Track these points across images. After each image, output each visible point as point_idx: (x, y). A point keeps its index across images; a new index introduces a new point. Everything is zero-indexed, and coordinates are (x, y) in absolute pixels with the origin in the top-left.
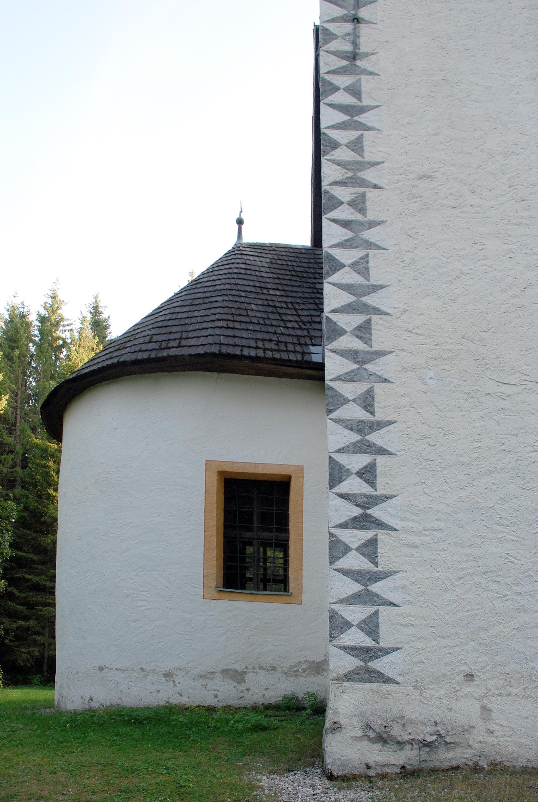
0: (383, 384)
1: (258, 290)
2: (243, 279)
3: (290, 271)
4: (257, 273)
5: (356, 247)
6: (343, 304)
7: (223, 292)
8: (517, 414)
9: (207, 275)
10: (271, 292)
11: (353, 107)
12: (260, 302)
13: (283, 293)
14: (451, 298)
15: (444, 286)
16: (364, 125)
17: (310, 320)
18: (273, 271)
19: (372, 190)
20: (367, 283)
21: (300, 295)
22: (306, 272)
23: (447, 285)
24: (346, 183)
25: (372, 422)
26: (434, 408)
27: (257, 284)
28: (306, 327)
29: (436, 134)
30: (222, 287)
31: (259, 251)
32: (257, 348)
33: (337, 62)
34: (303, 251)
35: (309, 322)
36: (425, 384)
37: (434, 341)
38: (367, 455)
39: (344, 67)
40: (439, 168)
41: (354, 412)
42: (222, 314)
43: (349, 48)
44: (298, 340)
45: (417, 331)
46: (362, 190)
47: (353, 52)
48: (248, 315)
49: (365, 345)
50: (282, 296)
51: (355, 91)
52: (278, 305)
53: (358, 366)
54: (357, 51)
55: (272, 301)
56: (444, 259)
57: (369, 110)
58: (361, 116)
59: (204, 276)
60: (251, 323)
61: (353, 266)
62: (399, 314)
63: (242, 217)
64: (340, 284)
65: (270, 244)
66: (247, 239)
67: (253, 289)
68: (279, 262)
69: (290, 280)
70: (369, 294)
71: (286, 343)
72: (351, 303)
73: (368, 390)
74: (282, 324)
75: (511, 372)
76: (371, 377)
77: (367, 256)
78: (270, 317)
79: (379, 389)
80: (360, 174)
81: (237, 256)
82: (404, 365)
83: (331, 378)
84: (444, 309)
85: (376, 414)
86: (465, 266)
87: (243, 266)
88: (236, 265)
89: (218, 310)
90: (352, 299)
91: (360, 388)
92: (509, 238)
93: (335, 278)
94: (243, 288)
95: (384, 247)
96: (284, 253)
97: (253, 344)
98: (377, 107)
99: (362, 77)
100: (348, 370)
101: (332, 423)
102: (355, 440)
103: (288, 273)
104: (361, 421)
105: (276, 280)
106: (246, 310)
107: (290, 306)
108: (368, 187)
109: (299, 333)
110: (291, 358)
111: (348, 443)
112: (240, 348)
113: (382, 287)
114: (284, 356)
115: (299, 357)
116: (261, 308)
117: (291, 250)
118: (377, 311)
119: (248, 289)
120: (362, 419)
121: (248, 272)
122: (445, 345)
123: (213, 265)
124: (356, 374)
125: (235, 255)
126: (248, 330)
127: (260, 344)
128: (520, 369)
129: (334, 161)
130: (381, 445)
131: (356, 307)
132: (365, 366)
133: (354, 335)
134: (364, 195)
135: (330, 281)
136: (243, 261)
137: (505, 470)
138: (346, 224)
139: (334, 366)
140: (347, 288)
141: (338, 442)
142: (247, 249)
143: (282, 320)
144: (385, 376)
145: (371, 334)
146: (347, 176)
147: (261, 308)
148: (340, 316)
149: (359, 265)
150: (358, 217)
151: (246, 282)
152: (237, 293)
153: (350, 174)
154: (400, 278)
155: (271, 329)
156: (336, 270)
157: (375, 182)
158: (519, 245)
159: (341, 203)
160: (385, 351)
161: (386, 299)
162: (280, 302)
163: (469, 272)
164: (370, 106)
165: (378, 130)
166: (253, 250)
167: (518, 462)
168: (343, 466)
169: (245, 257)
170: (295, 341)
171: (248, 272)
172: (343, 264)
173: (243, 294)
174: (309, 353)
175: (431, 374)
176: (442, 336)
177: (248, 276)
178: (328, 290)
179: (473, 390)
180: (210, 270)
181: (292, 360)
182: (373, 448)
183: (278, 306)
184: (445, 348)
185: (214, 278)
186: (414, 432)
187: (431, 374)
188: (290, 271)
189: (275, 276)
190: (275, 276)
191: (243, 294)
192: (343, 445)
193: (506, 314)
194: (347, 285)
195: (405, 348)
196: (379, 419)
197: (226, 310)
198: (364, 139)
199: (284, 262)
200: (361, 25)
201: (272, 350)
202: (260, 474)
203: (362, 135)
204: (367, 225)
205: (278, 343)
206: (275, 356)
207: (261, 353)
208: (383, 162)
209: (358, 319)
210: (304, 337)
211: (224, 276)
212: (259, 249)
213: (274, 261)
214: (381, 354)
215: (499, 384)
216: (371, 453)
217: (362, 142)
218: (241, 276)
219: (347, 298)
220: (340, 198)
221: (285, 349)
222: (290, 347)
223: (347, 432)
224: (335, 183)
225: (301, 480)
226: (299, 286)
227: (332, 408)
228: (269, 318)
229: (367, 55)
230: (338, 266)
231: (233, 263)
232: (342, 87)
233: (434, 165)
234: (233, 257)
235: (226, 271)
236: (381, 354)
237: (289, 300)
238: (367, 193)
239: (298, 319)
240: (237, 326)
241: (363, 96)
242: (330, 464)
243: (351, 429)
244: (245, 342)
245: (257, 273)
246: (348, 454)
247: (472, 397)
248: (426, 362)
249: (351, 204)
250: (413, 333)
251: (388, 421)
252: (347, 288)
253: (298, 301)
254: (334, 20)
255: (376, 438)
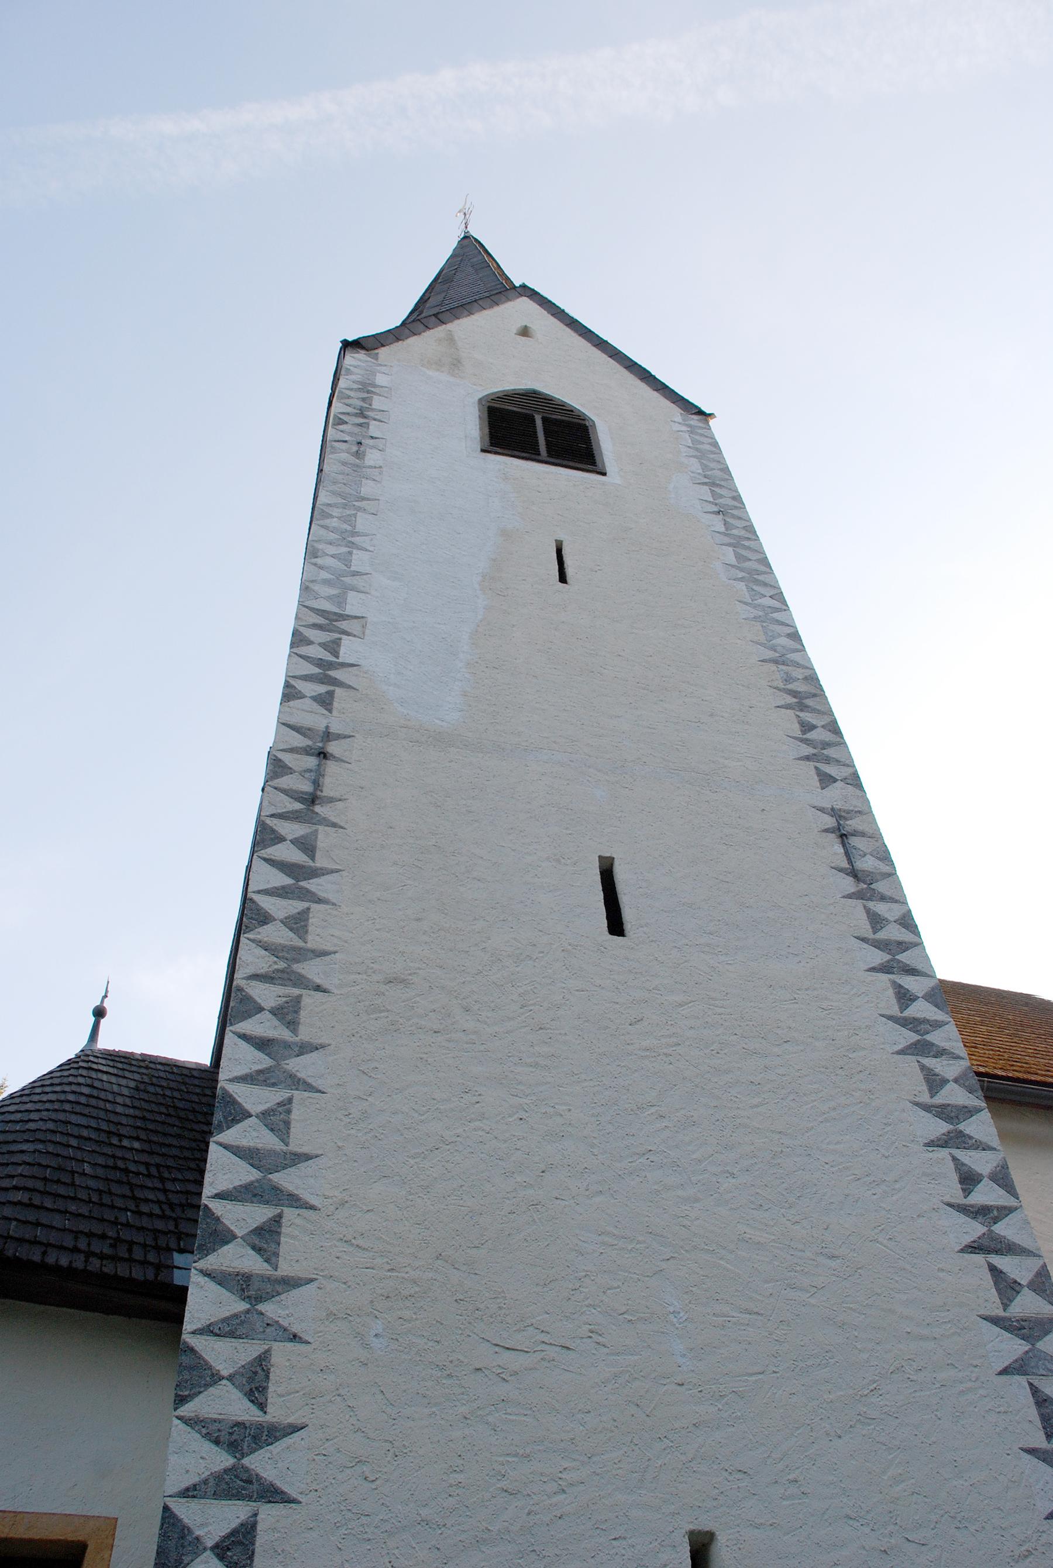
0: (290, 1345)
1: (103, 1137)
2: (81, 1114)
3: (167, 1107)
4: (108, 1106)
5: (274, 1085)
6: (237, 1183)
7: (40, 1136)
8: (529, 1412)
9: (17, 1100)
10: (126, 1143)
11: (300, 867)
12: (101, 1160)
13: (146, 1147)
14: (422, 1183)
15: (412, 1162)
16: (313, 894)
17: (184, 1202)
18: (137, 1103)
19: (312, 993)
20: (285, 1148)
21: (174, 1152)
22: (194, 1111)
23: (417, 1160)
24: (273, 978)
25: (260, 1427)
26: (380, 1397)
27: (104, 1126)
28: (174, 1215)
29: (418, 920)
30: (40, 1125)
31: (120, 1065)
32: (75, 1250)
33: (287, 804)
34: (195, 1073)
35: (181, 1205)
36: (366, 1346)
37: (388, 1263)
38: (241, 1502)
39: (296, 811)
40: (420, 969)
41: (226, 1403)
42: (25, 1176)
43: (307, 787)
44: (156, 1239)
45: (360, 1242)
46: (296, 991)
47: (311, 794)
48: (73, 1184)
49: (266, 1264)
50: (143, 1151)
51: (307, 846)
52: (132, 1167)
53: (248, 1306)
54: (319, 793)
55: (123, 1159)
56: (416, 1115)
57: (323, 875)
58: (311, 881)
59: (14, 1101)
60: (74, 1199)
61: (265, 1116)
62: (332, 1208)
63: (105, 1005)
64: (238, 1147)
65: (142, 1054)
66: (104, 1043)
67: (94, 1135)
68: (151, 1089)
69: (163, 1123)
70: (284, 1168)
71: (131, 1244)
72: (251, 1183)
73: (260, 1356)
74: (131, 1205)
75: (518, 1327)
76: (269, 1330)
77: (290, 1100)
78: (113, 1190)
79: (282, 1354)
80: (297, 967)
81: (81, 1071)
82: (332, 1308)
83: (195, 1327)
84: (409, 1203)
85: (269, 1409)
86: (447, 1128)
87: (86, 1090)
88: (74, 1088)
89: (20, 1170)
90: (253, 1175)
91: (244, 1352)
92: (519, 1087)
93: (231, 1135)
94: (75, 1131)
95: (320, 1088)
96: (162, 1074)
97: (69, 1242)
98: (337, 871)
99: (321, 828)
100: (228, 1314)
101: (182, 1426)
102: (223, 1466)
103: (163, 1110)
104: (238, 1424)
105: (138, 1120)
106: (73, 1172)
107: (154, 1171)
108: (306, 988)
109: (160, 1225)
110: (134, 1275)
111: (207, 1473)
112: (43, 1249)
113: (308, 1157)
114: (122, 1270)
115: (150, 1275)
116: (100, 1172)
117: (175, 1070)
118: (295, 1201)
119: (85, 1133)
120: (240, 1419)
121: (93, 1102)
122: (407, 1269)
123: (34, 1082)
124: (242, 1323)
125: (78, 1068)
126: (66, 1212)
127: (82, 1244)
128: (534, 1321)
129: (259, 943)
130: (270, 1479)
131: (259, 1191)
132: (260, 1307)
133: (249, 1245)
134: (298, 999)
135: (221, 1140)
136: (89, 1081)
137: (507, 1537)
138: (262, 1044)
139: (205, 1302)
140: (248, 1155)
141: (187, 1471)
142: (100, 1061)
143: (134, 1198)
144: (295, 1328)
145: (279, 1244)
146: (276, 967)
147: (100, 1172)
148: (229, 1205)
149: (274, 1115)
150: (285, 1034)
151: (83, 1121)
152: (64, 1139)
153: (281, 965)
154: (340, 1144)
155: (109, 1215)
156: (235, 1121)
157: (318, 981)
158: (534, 1098)
159: (261, 1009)
160: (300, 1279)
161: (312, 1181)
162: (135, 1162)
163: (454, 1139)
164: (326, 869)
165: (334, 904)
166: (111, 1063)
167: (531, 1517)
168: (189, 1529)
169: (94, 1075)
170: (150, 1241)
171: (93, 1102)
172: (248, 1112)
173: (74, 1142)
174: (168, 1267)
175: (378, 1326)
176: (402, 1253)
177: (92, 1110)
178: (215, 1154)
179: (451, 1362)
180: (26, 1092)
181: (135, 1280)
182: (255, 1487)
183: (133, 1169)
184: (406, 1276)
185: (29, 1106)
186: (338, 1451)
187: (378, 1326)
188: (167, 1107)
189: (137, 1113)
190: (137, 1113)
191: (74, 1142)
192: (196, 1479)
193: (511, 1216)
194: (249, 1149)
195: (337, 1274)
196: (275, 1420)
197: (35, 1171)
198: (311, 915)
199: (159, 1090)
200: (328, 762)
201: (102, 1257)
202: (21, 1540)
203: (308, 909)
204: (296, 1049)
205: (117, 1241)
206: (105, 1270)
207: (79, 1263)
208: (335, 952)
209: (258, 1214)
210: (165, 1233)
211: (48, 1106)
212: (123, 1062)
213: (142, 1086)
214: (291, 1283)
215: (497, 1349)
216: (250, 1498)
217: (307, 920)
218: (78, 1109)
219: (245, 1174)
220: (259, 1001)
221: (126, 1256)
222: (138, 1254)
223: (208, 1447)
224: (255, 977)
225: (106, 1556)
226: (179, 1136)
227: (186, 1393)
228: (110, 1193)
229: (331, 800)
230: (238, 1114)
231: (70, 1084)
232: (290, 837)
233: (411, 964)
234: (72, 1072)
235: (53, 1097)
236: (291, 1283)
237: (157, 1160)
238: (304, 998)
239: (162, 1197)
240: (48, 1203)
241: (318, 854)
242: (162, 1525)
243: (217, 1442)
244: (53, 1238)
245: (108, 1106)
246: (202, 1501)
247: (450, 1376)
248: (372, 1302)
249: (276, 1012)
250: (352, 1245)
251: (290, 1425)
252: (248, 1155)
253: (170, 1162)
254: (292, 750)
255: (263, 1463)
